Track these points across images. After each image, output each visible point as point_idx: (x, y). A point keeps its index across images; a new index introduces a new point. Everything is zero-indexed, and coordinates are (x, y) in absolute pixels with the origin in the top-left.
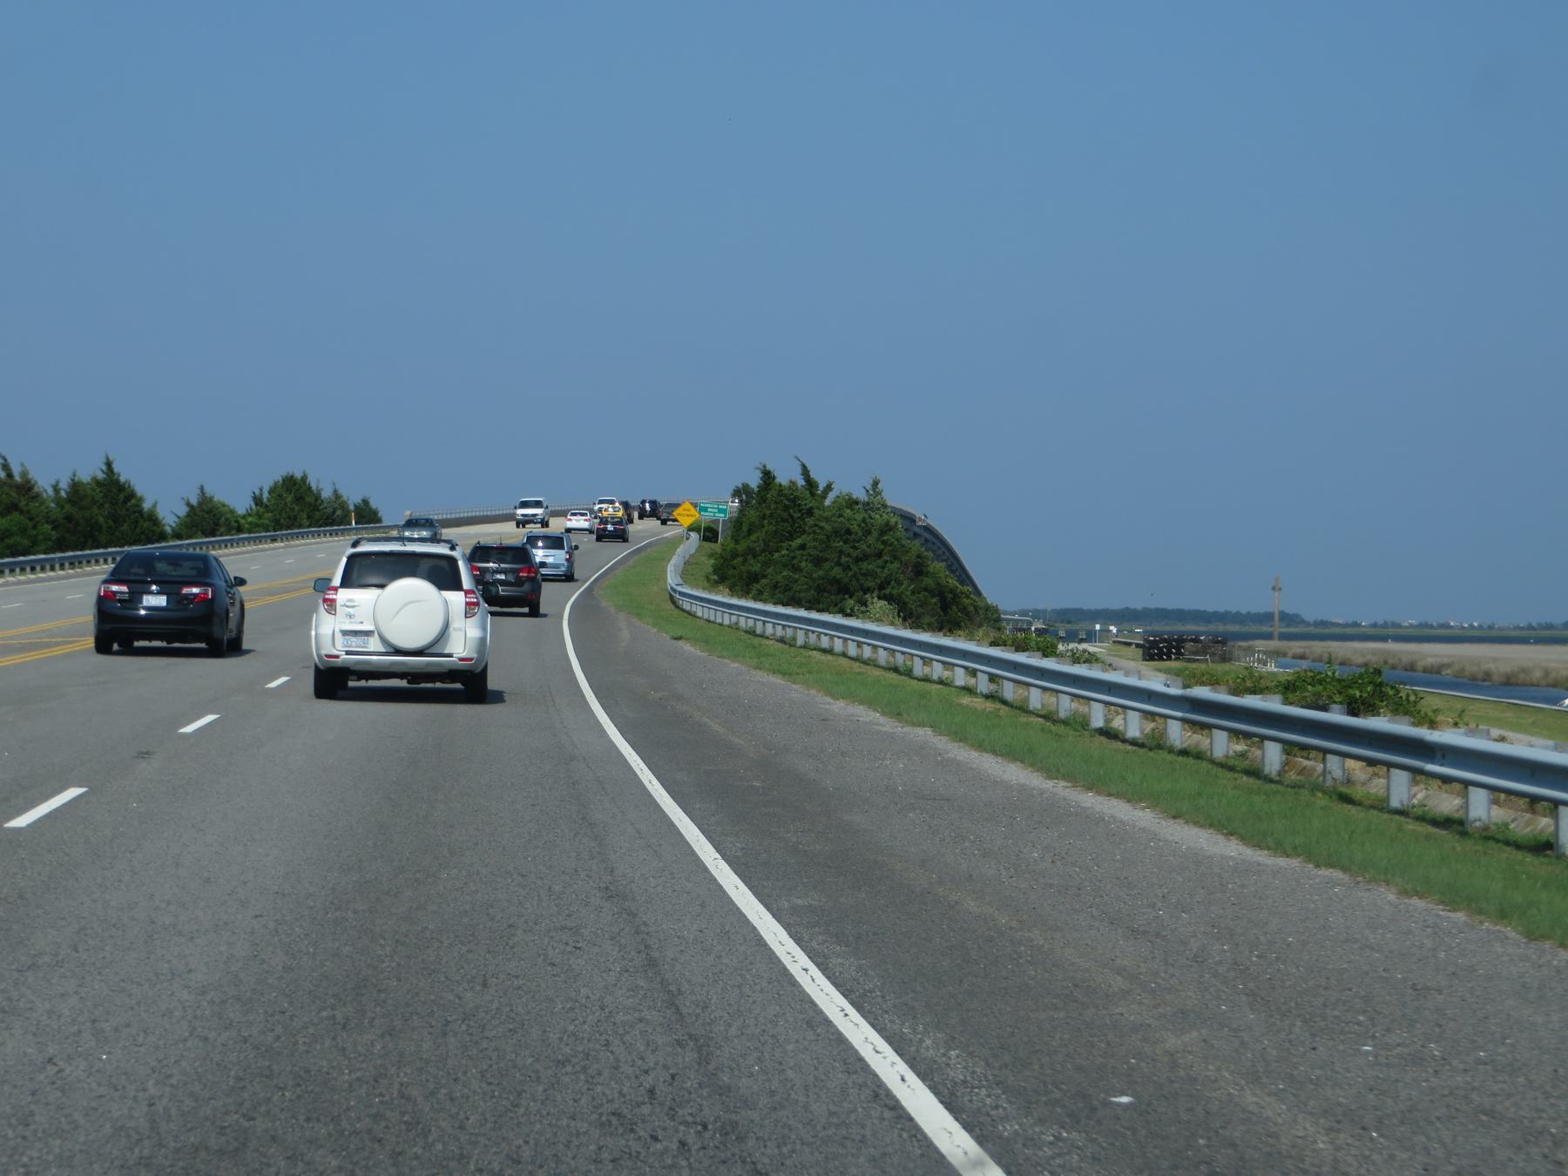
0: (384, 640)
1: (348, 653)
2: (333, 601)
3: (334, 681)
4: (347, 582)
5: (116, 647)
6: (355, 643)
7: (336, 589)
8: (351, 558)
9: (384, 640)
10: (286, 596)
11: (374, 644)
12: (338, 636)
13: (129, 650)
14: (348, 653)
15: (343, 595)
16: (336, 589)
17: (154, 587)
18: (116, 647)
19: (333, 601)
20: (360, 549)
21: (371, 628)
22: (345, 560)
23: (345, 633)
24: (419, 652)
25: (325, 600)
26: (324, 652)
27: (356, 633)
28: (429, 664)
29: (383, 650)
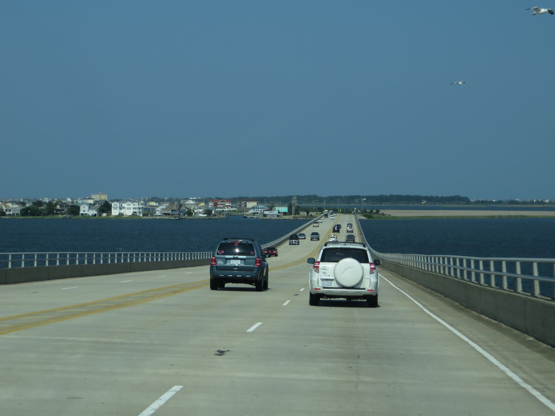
0: (338, 282)
1: (324, 288)
3: (317, 299)
4: (323, 260)
6: (327, 284)
7: (319, 262)
8: (325, 250)
9: (338, 282)
10: (332, 299)
11: (334, 284)
12: (320, 281)
14: (324, 288)
15: (322, 265)
16: (319, 262)
19: (318, 267)
21: (333, 278)
23: (322, 280)
25: (314, 267)
26: (314, 287)
27: (327, 280)
28: (356, 292)
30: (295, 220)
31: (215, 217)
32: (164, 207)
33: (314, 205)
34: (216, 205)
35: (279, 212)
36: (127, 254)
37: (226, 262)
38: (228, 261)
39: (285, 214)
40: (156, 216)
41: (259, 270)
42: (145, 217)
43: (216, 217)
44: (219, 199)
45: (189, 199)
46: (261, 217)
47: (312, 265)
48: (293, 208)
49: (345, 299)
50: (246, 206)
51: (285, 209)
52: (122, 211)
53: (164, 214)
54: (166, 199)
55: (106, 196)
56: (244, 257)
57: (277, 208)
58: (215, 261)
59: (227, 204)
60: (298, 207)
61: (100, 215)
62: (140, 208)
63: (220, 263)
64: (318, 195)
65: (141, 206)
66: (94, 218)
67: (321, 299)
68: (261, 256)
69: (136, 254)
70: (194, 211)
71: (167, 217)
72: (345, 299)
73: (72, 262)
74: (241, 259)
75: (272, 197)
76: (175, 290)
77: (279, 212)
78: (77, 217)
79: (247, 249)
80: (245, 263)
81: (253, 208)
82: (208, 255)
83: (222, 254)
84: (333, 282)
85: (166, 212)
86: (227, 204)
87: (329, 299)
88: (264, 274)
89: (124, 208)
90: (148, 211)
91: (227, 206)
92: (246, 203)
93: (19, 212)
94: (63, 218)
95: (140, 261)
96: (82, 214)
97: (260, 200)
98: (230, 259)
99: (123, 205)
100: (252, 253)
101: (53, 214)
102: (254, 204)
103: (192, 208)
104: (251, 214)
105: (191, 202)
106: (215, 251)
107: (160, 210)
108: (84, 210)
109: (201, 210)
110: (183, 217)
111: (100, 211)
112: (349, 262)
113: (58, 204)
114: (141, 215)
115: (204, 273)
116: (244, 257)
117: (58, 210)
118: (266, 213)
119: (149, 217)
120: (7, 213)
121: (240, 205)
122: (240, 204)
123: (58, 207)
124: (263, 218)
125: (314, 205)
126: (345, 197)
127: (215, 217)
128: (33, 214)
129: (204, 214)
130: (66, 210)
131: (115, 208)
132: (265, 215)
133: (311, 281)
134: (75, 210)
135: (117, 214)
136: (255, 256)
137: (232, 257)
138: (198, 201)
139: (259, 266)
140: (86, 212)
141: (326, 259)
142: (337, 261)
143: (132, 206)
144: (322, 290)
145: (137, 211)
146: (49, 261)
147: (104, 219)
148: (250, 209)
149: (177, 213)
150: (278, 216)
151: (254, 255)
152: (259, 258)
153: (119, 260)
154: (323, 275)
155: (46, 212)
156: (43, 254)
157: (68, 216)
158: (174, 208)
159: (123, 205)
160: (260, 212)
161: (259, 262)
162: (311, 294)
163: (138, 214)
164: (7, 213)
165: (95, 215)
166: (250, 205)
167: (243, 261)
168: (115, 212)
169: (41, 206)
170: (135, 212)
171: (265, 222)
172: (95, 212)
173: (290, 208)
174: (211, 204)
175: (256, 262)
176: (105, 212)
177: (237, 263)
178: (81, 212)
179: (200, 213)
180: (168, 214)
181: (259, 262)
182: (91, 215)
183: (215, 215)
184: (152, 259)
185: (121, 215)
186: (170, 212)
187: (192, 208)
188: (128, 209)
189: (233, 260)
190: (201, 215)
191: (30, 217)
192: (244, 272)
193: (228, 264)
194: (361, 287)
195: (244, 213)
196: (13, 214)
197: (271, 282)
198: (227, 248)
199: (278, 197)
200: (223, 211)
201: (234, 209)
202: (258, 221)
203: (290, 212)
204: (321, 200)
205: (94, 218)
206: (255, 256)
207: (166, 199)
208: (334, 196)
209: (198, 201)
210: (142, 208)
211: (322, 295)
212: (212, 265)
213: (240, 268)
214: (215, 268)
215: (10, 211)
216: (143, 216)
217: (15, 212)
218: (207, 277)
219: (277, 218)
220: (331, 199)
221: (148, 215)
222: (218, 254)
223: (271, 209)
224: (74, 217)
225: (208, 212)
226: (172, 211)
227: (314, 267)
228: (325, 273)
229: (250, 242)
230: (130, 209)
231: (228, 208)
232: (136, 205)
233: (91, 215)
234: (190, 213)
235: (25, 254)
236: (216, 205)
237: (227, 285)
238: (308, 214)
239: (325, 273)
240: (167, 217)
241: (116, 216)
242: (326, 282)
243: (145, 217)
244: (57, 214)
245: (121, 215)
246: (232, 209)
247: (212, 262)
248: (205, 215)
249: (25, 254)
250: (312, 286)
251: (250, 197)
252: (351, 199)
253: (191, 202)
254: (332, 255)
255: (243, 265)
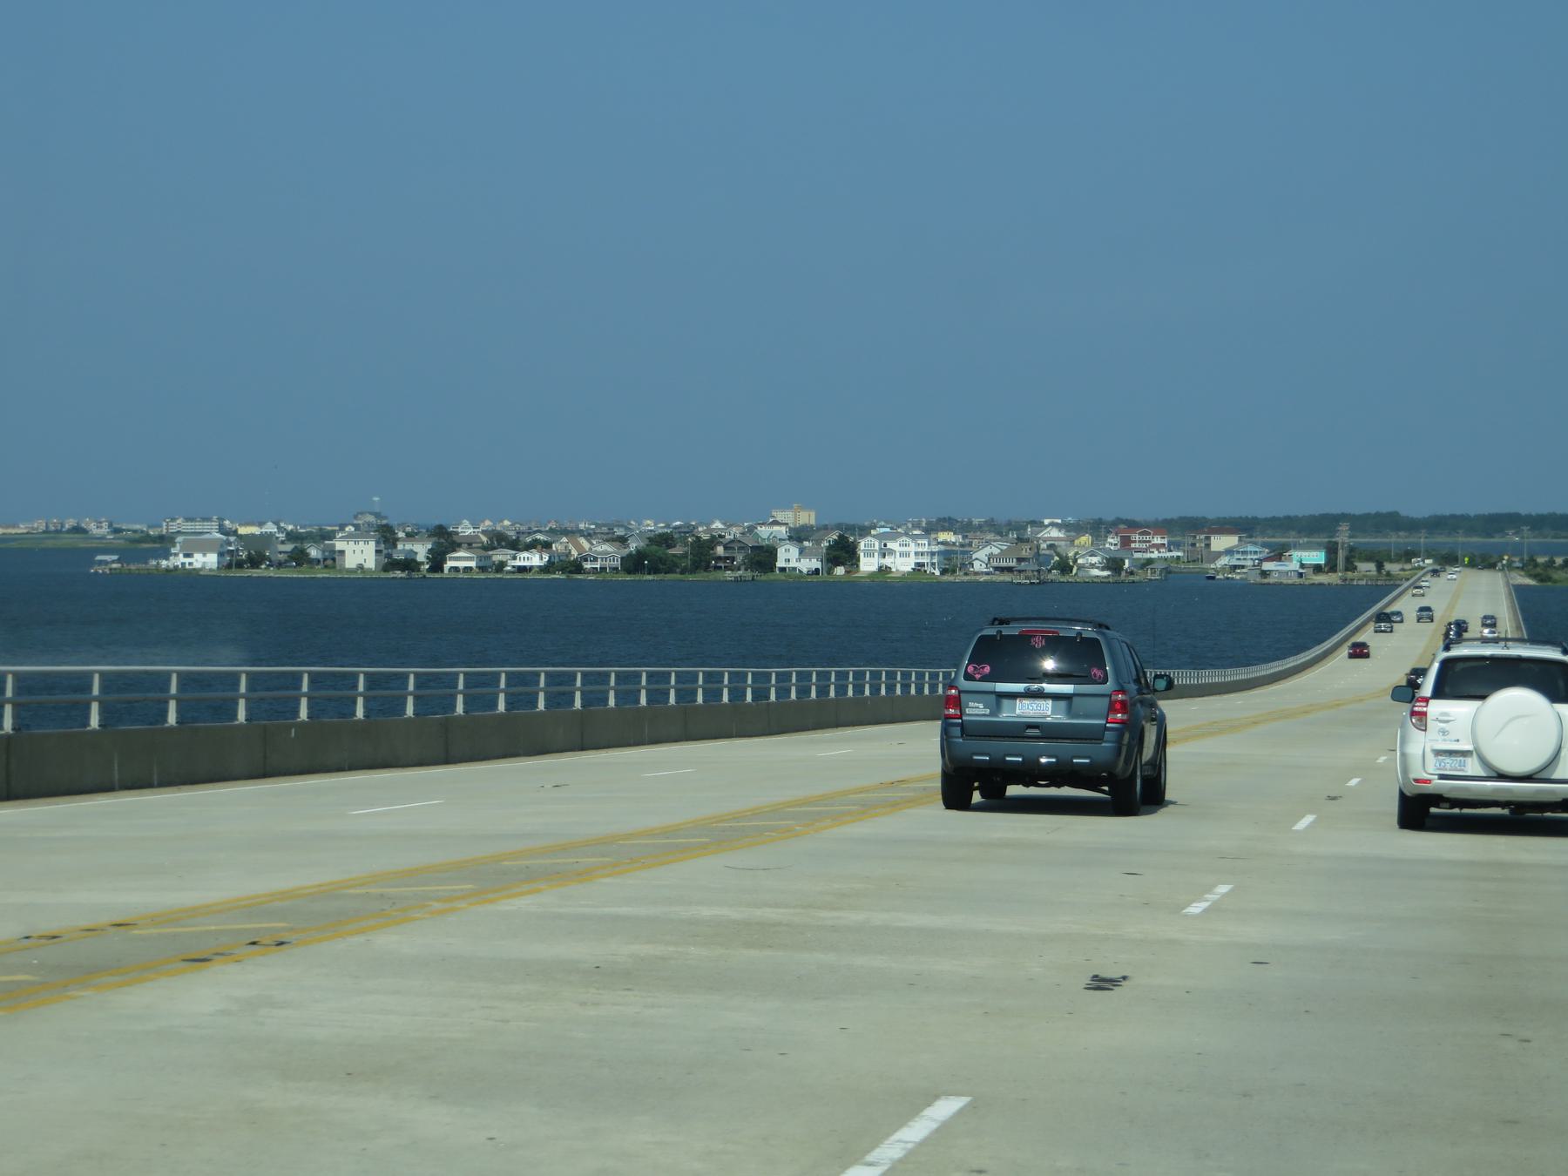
0: (1484, 762)
1: (1442, 777)
2: (1425, 714)
3: (1418, 811)
4: (1439, 693)
5: (977, 797)
6: (1450, 767)
7: (1426, 700)
8: (1447, 664)
9: (1484, 762)
10: (1466, 811)
11: (1473, 767)
12: (1430, 757)
13: (998, 802)
14: (1442, 777)
15: (1436, 708)
16: (1426, 700)
17: (1049, 664)
18: (977, 797)
19: (1425, 714)
20: (1456, 652)
21: (1469, 747)
22: (1436, 665)
23: (1438, 753)
24: (1528, 778)
25: (1413, 713)
26: (1413, 775)
27: (1451, 753)
28: (1539, 791)
29: (1483, 774)
30: (1346, 586)
31: (1131, 578)
32: (996, 551)
33: (1395, 539)
34: (1126, 542)
35: (1302, 566)
36: (910, 674)
37: (997, 709)
38: (1006, 702)
39: (1317, 569)
40: (976, 573)
41: (1121, 736)
42: (948, 578)
43: (1136, 578)
44: (1133, 525)
45: (1042, 526)
46: (1254, 578)
47: (1408, 706)
48: (1341, 555)
49: (1506, 812)
50: (1208, 546)
51: (1318, 557)
52: (888, 561)
53: (996, 569)
54: (976, 521)
55: (813, 515)
56: (1068, 688)
57: (1297, 555)
58: (956, 702)
59: (1158, 540)
60: (1352, 549)
61: (830, 572)
62: (933, 554)
63: (976, 710)
64: (1403, 513)
65: (936, 549)
66: (815, 579)
67: (1433, 810)
68: (1133, 687)
69: (707, 676)
70: (1075, 561)
71: (1006, 577)
72: (1506, 812)
73: (713, 694)
74: (1056, 697)
75: (1274, 519)
76: (491, 877)
77: (1302, 566)
78: (770, 576)
79: (1083, 658)
80: (1070, 712)
81: (1229, 552)
82: (924, 682)
83: (984, 679)
84: (1469, 760)
85: (1003, 564)
86: (1158, 540)
87: (1456, 811)
88: (1148, 752)
89: (892, 552)
90: (952, 560)
91: (1158, 547)
92: (1208, 538)
93: (617, 564)
94: (736, 580)
95: (898, 692)
96: (783, 570)
97: (1244, 527)
98: (1013, 696)
99: (890, 545)
100: (1095, 671)
101: (707, 568)
102: (1230, 541)
103: (1071, 554)
104: (1223, 569)
105: (1055, 533)
106: (957, 666)
107: (984, 558)
108: (789, 557)
109: (1094, 560)
110: (1050, 577)
111: (828, 560)
112: (1518, 704)
113: (720, 543)
114: (937, 573)
115: (918, 749)
116: (1068, 688)
117: (719, 559)
118: (1267, 566)
119: (959, 577)
120: (588, 566)
121: (1193, 545)
122: (1191, 541)
123: (720, 550)
124: (1259, 580)
125: (1395, 539)
126: (1477, 517)
127: (1131, 578)
128: (654, 570)
129: (1103, 569)
130: (739, 558)
131: (870, 554)
132: (1265, 574)
133: (1403, 755)
134: (763, 557)
135: (874, 568)
136: (1110, 686)
137: (1019, 687)
138: (1074, 529)
139: (1122, 722)
140: (792, 565)
141: (1447, 690)
142: (1483, 697)
143: (912, 548)
144: (1438, 786)
145: (925, 560)
146: (677, 691)
147: (839, 583)
148: (1219, 555)
149: (1031, 566)
150: (1301, 575)
151: (1105, 681)
152: (1123, 691)
153: (841, 690)
154: (1440, 737)
155: (687, 563)
156: (663, 673)
157: (749, 574)
158: (1024, 554)
159: (890, 545)
160: (1249, 563)
161: (1124, 707)
162: (1402, 795)
163: (929, 569)
164: (588, 566)
165: (817, 570)
166: (1220, 543)
167: (1062, 704)
168: (868, 565)
169: (669, 547)
170: (922, 565)
171: (1268, 592)
172: (815, 564)
173: (1331, 551)
174: (1112, 542)
175: (1112, 708)
176: (842, 564)
177: (1041, 711)
178: (780, 563)
179: (1093, 566)
180: (1010, 570)
181: (1124, 707)
182: (805, 571)
183: (1132, 573)
184: (875, 689)
185: (883, 570)
186: (1013, 564)
187: (1071, 554)
188: (898, 555)
189: (1026, 702)
190: (1096, 572)
191: (650, 577)
192: (1066, 747)
193: (1005, 716)
194: (1556, 776)
195: (1205, 566)
196: (603, 569)
197: (1175, 784)
198: (1004, 655)
199: (1288, 518)
200: (1150, 561)
201: (1175, 554)
202: (1246, 588)
203: (1331, 566)
204: (1412, 525)
205: (815, 579)
206: (1110, 686)
207: (976, 521)
208: (1447, 513)
209: (1074, 529)
210: (939, 553)
211: (1437, 799)
212: (948, 717)
213: (1049, 732)
214: (957, 731)
215: (595, 559)
216: (944, 572)
217: (607, 564)
218: (933, 766)
219: (1298, 581)
220: (1437, 524)
221: (954, 571)
222: (968, 677)
223: (1278, 554)
224: (764, 578)
225: (1114, 564)
226: (1020, 560)
227: (1413, 713)
228: (1444, 732)
229: (1089, 632)
230: (907, 555)
231: (1157, 549)
232: (924, 545)
233: (805, 571)
234: (1064, 567)
235: (547, 673)
236: (1126, 542)
237: (1013, 790)
238: (1380, 567)
239: (1444, 732)
240: (1006, 577)
241: (872, 574)
242: (1448, 760)
243: (948, 578)
244: (717, 568)
245: (883, 570)
246: (1169, 554)
247: (945, 711)
248: (1106, 573)
249: (547, 673)
250: (1405, 770)
251: (1211, 514)
252: (1496, 523)
253: (1055, 533)
254: (1467, 679)
255: (1061, 718)
